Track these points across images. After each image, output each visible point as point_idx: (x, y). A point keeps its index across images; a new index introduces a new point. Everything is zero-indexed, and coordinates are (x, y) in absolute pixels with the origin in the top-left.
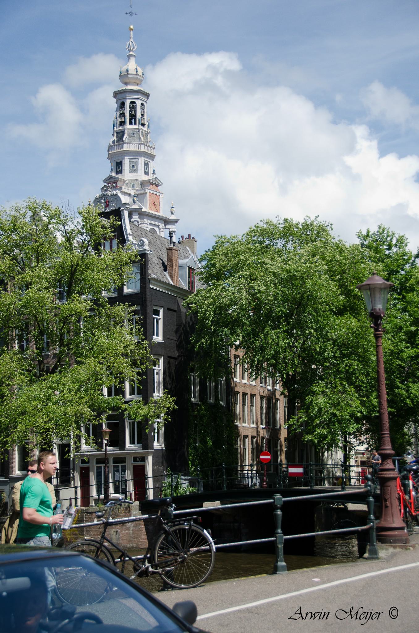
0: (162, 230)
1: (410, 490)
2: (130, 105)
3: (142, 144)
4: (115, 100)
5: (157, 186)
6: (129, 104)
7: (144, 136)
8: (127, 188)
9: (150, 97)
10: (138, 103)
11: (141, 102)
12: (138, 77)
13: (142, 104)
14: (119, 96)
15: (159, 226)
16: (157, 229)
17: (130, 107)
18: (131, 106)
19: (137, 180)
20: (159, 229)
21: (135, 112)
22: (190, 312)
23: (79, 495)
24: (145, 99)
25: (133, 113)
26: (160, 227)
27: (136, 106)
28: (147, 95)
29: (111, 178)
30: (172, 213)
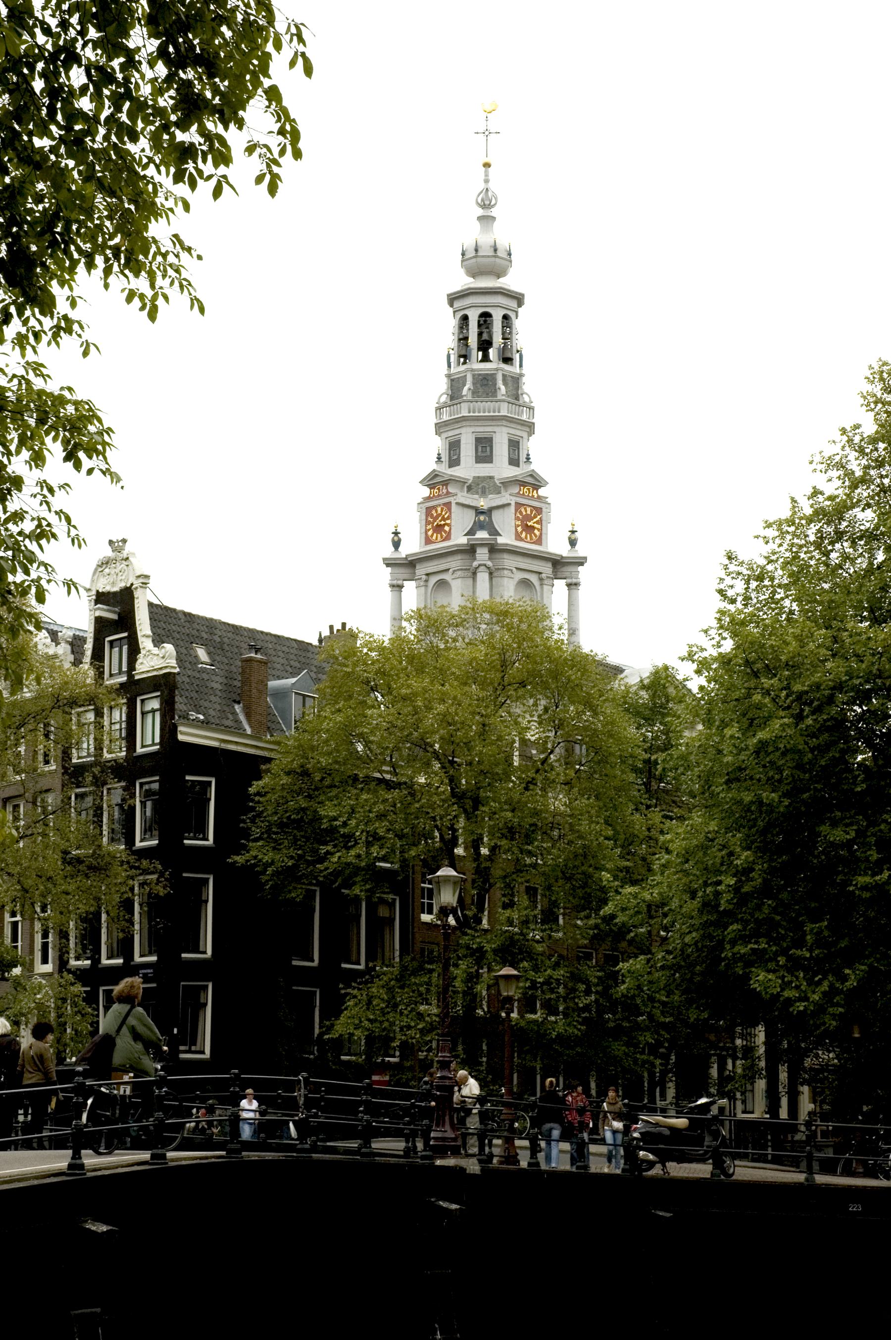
0: (546, 582)
1: (148, 1054)
2: (479, 321)
3: (504, 401)
4: (451, 310)
5: (536, 487)
6: (477, 318)
7: (510, 384)
8: (470, 496)
9: (526, 300)
10: (497, 316)
11: (502, 312)
12: (497, 260)
13: (505, 317)
14: (457, 304)
15: (540, 573)
16: (534, 579)
17: (479, 325)
18: (482, 322)
19: (491, 478)
20: (541, 579)
21: (490, 335)
22: (484, 1059)
23: (124, 718)
24: (513, 304)
25: (485, 337)
26: (543, 575)
27: (492, 321)
28: (519, 299)
29: (437, 476)
30: (573, 543)
